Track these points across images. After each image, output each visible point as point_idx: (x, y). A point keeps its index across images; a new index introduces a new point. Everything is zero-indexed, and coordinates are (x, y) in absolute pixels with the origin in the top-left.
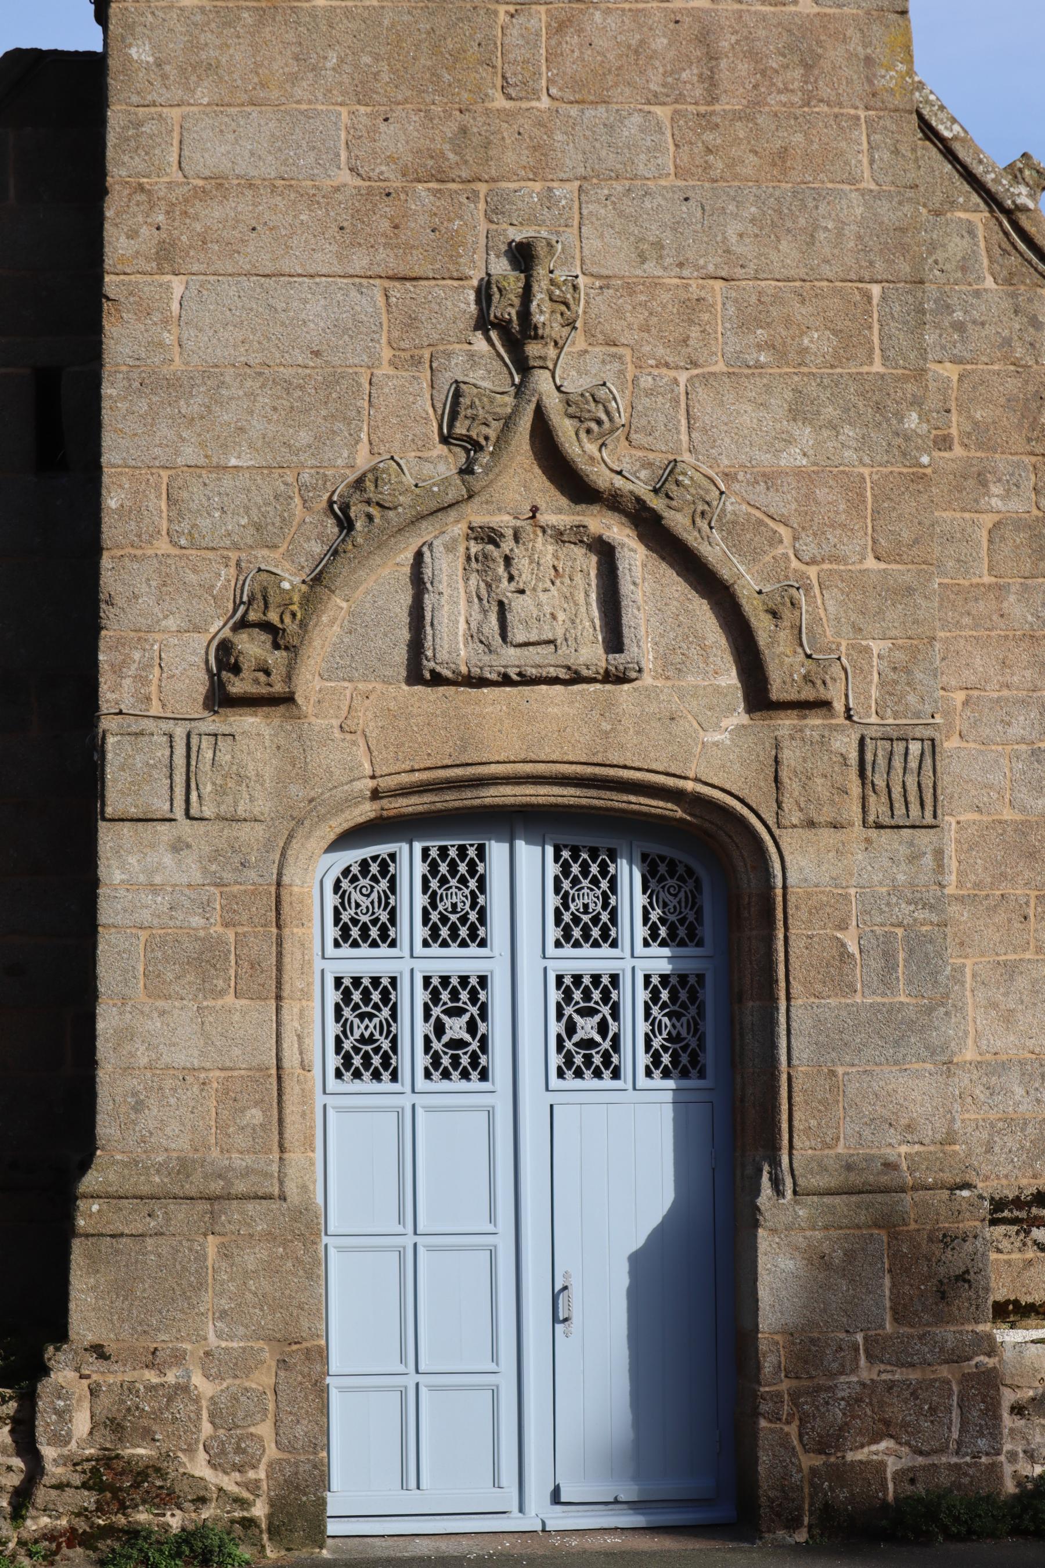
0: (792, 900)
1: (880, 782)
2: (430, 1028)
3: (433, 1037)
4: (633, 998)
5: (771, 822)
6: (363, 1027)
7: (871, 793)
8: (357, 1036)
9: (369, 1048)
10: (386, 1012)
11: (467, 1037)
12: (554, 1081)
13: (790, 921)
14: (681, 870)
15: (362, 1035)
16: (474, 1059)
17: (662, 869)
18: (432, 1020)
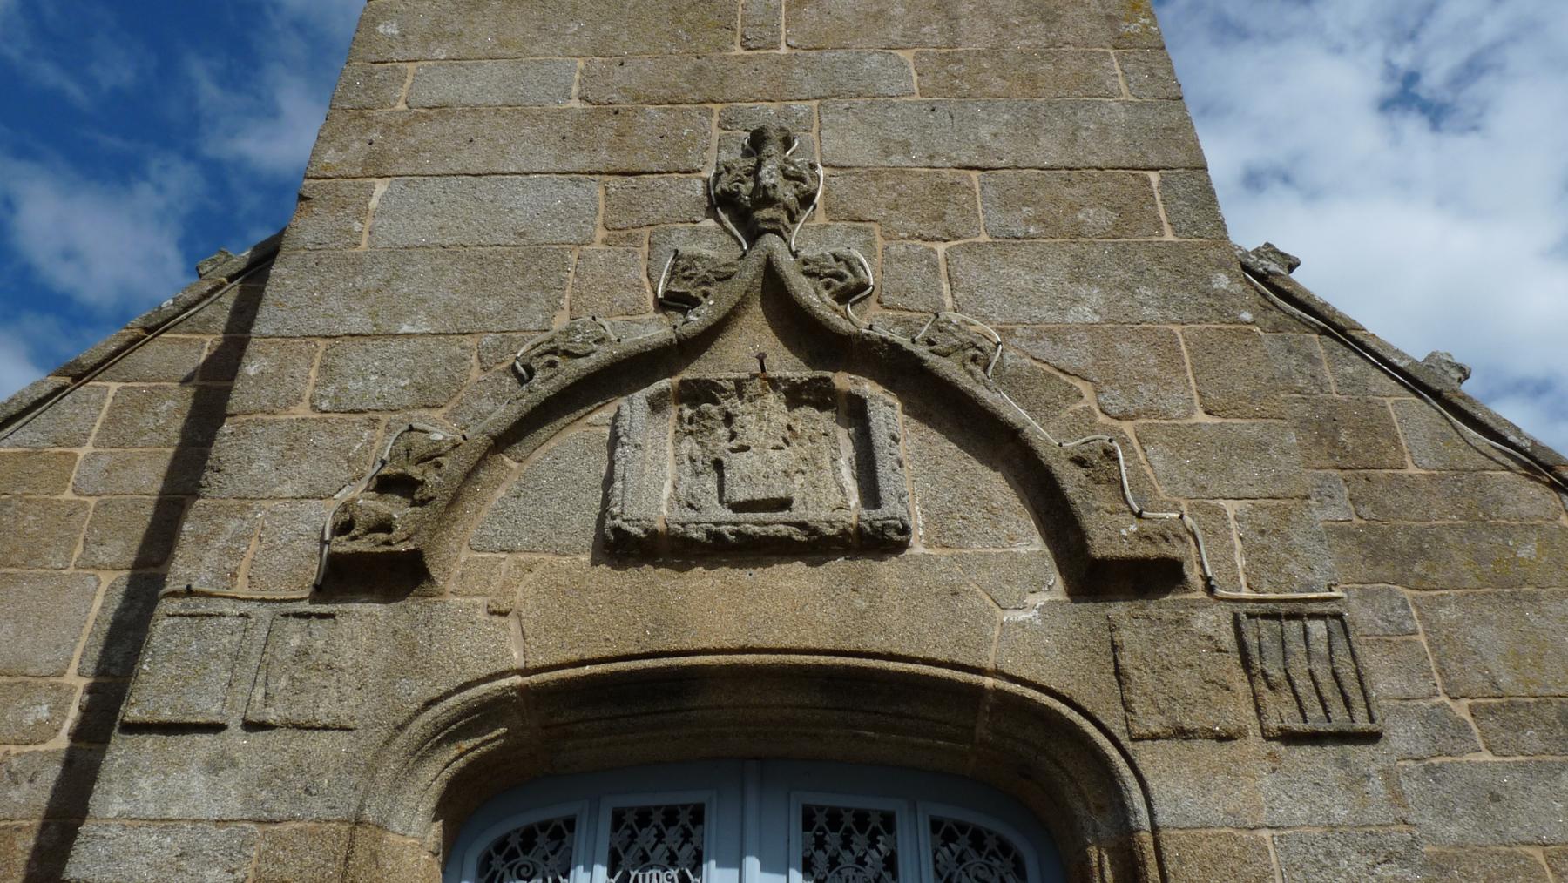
0: (1169, 849)
1: (1276, 674)
5: (1118, 730)
7: (1264, 688)
14: (991, 844)
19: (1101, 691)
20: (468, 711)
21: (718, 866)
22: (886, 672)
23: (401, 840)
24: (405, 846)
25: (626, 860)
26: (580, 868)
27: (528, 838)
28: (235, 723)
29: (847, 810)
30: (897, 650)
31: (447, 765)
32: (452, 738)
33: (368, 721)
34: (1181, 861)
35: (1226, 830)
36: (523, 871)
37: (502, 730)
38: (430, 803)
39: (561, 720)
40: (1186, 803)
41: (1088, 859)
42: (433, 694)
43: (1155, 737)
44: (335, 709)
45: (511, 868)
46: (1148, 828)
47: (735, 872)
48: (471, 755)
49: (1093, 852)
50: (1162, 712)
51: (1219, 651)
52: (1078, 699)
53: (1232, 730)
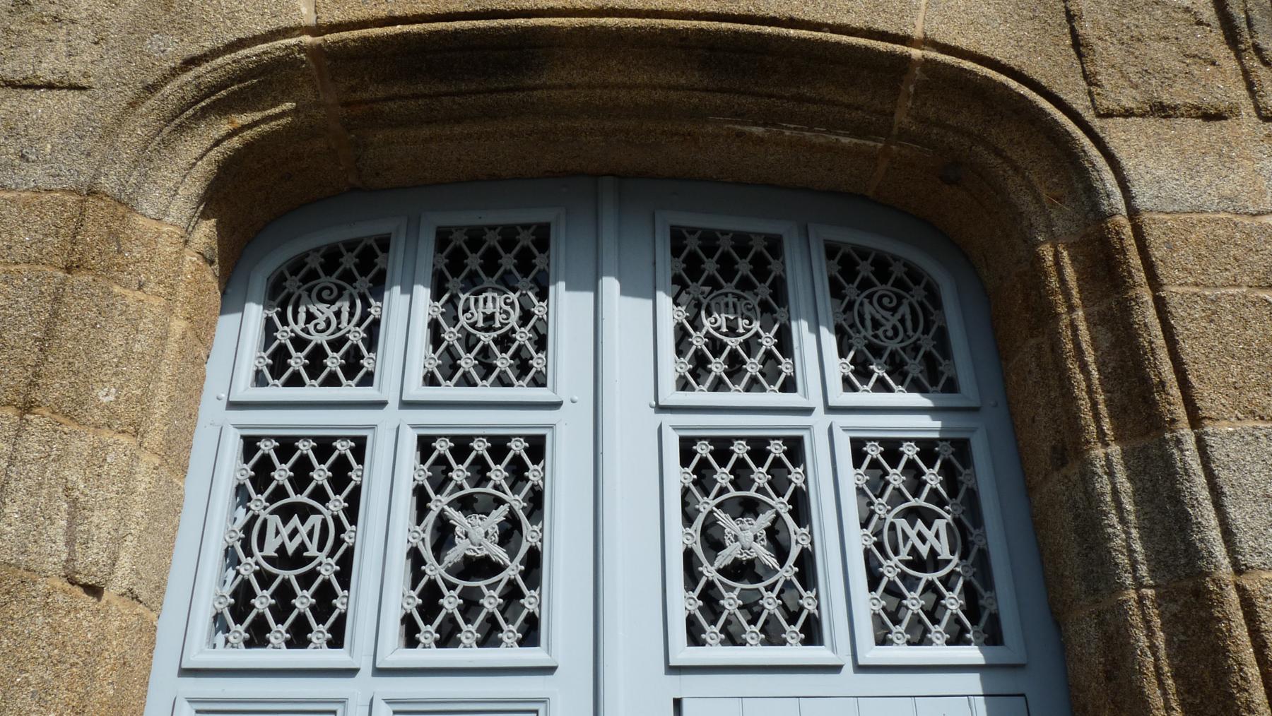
0: (1154, 235)
2: (424, 538)
3: (427, 553)
4: (832, 482)
5: (1081, 104)
6: (285, 532)
8: (270, 550)
9: (291, 575)
10: (337, 504)
11: (499, 554)
12: (685, 654)
13: (1161, 270)
14: (898, 271)
15: (282, 549)
16: (512, 594)
17: (865, 269)
18: (430, 519)
19: (1056, 64)
20: (243, 74)
21: (568, 288)
22: (787, 39)
23: (155, 225)
24: (159, 234)
25: (454, 283)
26: (397, 289)
27: (331, 258)
28: (366, 668)
29: (725, 233)
30: (798, 15)
31: (217, 143)
32: (223, 108)
33: (107, 79)
34: (1172, 249)
35: (1223, 215)
36: (325, 294)
37: (288, 105)
38: (194, 187)
39: (365, 96)
40: (1170, 185)
41: (1040, 259)
42: (195, 50)
43: (1128, 113)
44: (64, 64)
45: (310, 291)
46: (1124, 212)
47: (589, 296)
48: (248, 134)
49: (1047, 252)
50: (1136, 87)
51: (1199, 23)
52: (1028, 72)
53: (1222, 107)
